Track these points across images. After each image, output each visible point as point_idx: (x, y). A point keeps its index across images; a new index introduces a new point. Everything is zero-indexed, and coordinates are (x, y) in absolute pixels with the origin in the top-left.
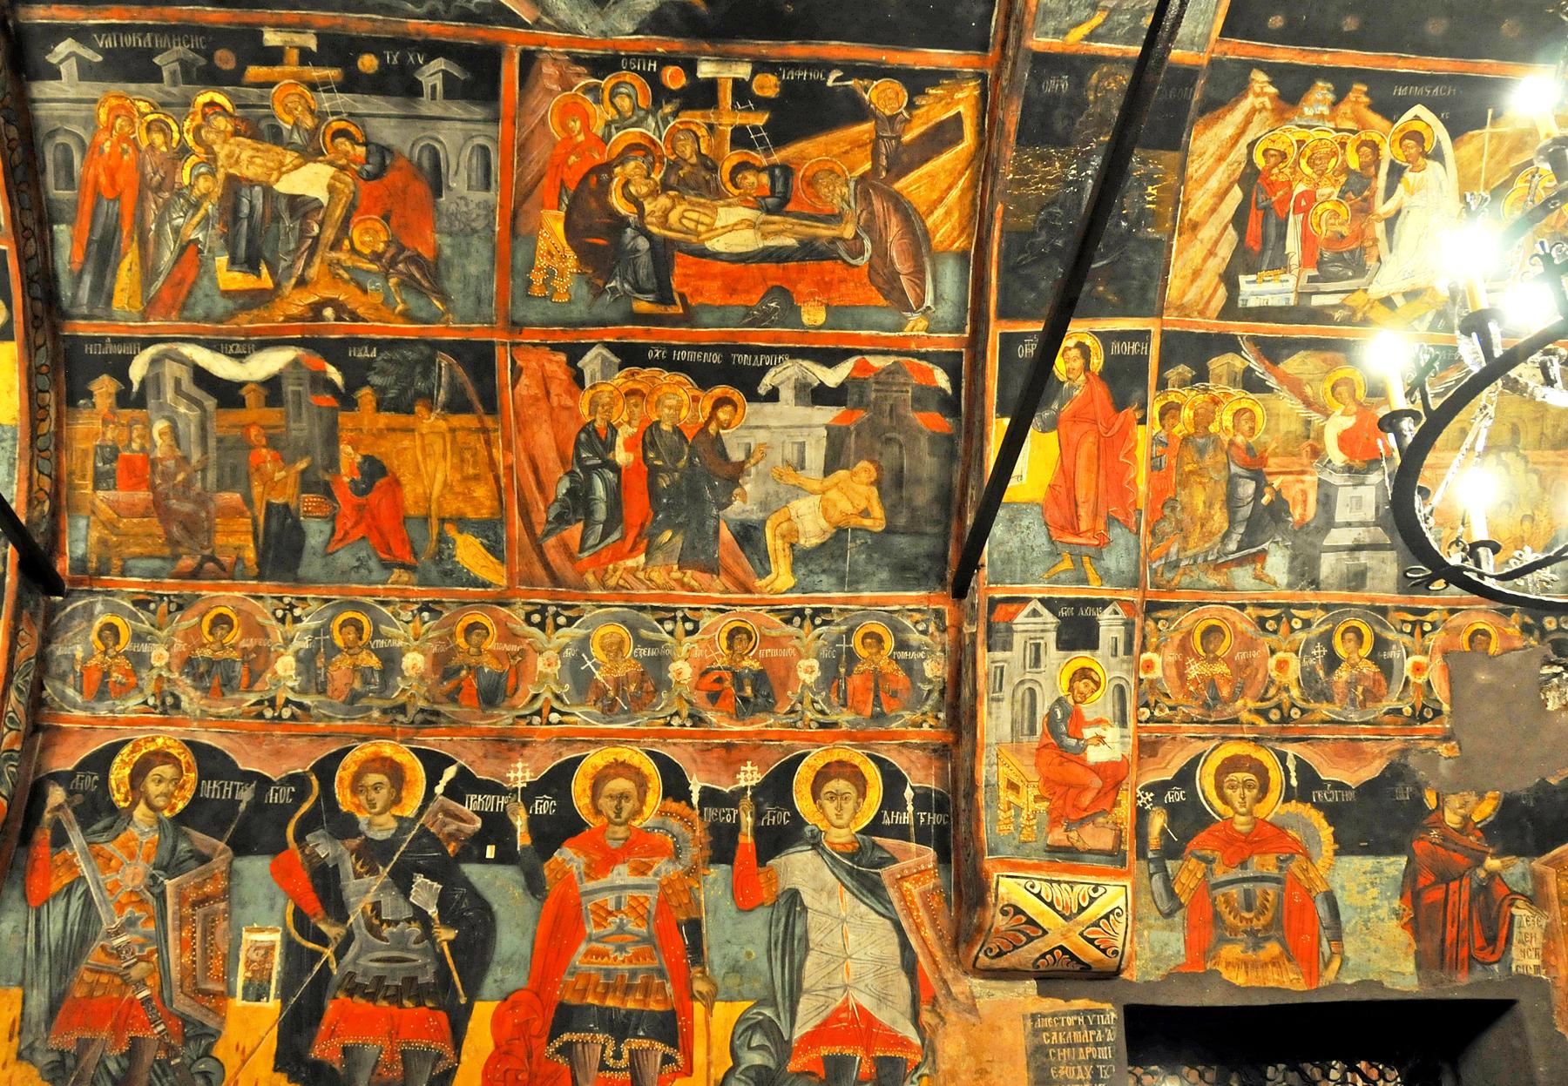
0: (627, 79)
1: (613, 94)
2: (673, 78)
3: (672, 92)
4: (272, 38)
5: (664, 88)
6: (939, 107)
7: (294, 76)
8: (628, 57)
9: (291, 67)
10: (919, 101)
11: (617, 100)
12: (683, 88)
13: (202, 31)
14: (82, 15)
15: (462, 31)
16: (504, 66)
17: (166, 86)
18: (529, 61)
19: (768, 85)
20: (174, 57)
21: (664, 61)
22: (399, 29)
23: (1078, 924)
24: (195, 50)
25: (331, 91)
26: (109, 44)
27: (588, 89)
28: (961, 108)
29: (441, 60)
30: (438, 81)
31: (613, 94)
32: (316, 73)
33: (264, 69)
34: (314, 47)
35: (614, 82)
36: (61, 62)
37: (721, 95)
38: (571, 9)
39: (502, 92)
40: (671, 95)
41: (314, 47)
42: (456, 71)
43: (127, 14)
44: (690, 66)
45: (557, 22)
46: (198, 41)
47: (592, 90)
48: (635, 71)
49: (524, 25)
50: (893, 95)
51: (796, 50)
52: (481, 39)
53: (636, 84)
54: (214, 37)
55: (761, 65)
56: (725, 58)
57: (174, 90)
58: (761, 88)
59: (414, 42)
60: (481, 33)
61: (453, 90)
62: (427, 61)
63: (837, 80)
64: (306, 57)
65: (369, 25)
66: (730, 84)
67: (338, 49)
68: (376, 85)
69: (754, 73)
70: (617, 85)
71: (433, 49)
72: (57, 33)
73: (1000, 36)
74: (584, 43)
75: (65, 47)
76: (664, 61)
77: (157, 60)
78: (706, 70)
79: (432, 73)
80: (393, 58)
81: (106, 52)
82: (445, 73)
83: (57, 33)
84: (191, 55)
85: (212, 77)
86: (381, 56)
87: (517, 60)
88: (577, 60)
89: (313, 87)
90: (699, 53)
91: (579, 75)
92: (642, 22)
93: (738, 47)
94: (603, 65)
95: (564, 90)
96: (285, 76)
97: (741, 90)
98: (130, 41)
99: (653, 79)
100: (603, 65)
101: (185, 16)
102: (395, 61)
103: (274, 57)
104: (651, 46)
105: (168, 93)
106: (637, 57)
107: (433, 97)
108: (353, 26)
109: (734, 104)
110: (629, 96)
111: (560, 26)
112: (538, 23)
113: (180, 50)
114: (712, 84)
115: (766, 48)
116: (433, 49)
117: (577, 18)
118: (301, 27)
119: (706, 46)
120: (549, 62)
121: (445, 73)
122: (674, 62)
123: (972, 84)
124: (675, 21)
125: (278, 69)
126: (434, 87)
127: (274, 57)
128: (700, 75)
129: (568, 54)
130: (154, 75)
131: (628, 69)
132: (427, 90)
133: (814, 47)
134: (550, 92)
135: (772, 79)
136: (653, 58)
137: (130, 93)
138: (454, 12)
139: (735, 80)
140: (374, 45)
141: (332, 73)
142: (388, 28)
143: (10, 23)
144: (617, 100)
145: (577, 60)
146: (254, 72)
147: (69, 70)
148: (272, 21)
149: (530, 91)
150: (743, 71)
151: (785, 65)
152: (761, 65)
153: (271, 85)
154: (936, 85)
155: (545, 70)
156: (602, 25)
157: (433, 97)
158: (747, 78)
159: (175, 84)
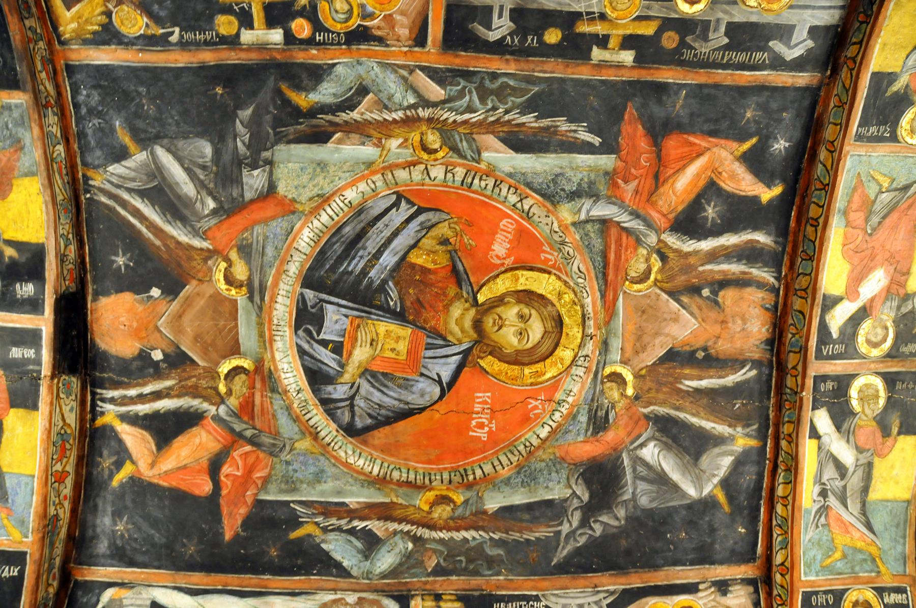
0: (339, 26)
1: (350, 11)
2: (301, 27)
3: (302, 16)
4: (628, 57)
5: (308, 19)
6: (86, 15)
7: (617, 26)
8: (339, 44)
9: (616, 34)
10: (104, 19)
11: (346, 7)
12: (293, 19)
13: (682, 63)
14: (770, 78)
15: (473, 63)
16: (440, 35)
17: (726, 19)
18: (420, 39)
19: (225, 24)
20: (710, 44)
21: (310, 42)
22: (523, 65)
23: (472, 504)
24: (692, 48)
25: (588, 13)
26: (759, 55)
27: (371, 16)
28: (68, 15)
29: (491, 39)
30: (496, 21)
31: (350, 11)
32: (599, 28)
33: (640, 32)
34: (595, 48)
35: (350, 23)
36: (805, 40)
37: (262, 14)
38: (385, 83)
39: (443, 12)
40: (302, 13)
41: (595, 48)
42: (480, 30)
43: (736, 78)
44: (290, 38)
45: (396, 72)
46: (687, 55)
47: (366, 16)
48: (333, 33)
49: (423, 69)
50: (126, 22)
51: (208, 57)
52: (457, 56)
53: (331, 21)
54: (675, 58)
55: (232, 41)
56: (261, 47)
57: (720, 15)
58: (230, 23)
59: (512, 53)
60: (458, 61)
61: (485, 14)
62: (504, 38)
63: (172, 33)
64: (603, 41)
65: (547, 67)
66: (256, 25)
67: (577, 47)
68: (549, 18)
69: (238, 35)
70: (347, 20)
71: (498, 48)
72: (798, 65)
73: (60, 79)
74: (375, 55)
75: (791, 54)
76: (310, 42)
77: (726, 40)
78: (276, 36)
79: (501, 27)
80: (531, 40)
81: (764, 48)
82: (489, 28)
83: (798, 65)
84: (696, 45)
85: (685, 26)
86: (541, 41)
87: (430, 39)
88: (381, 40)
89: (603, 17)
90: (284, 50)
91: (379, 28)
92: (330, 74)
93: (253, 57)
94: (359, 36)
95: (391, 15)
96: (624, 26)
97: (246, 20)
98: (742, 57)
99: (318, 26)
100: (359, 36)
101: (691, 75)
102: (530, 38)
103: (629, 42)
104: (321, 54)
105: (725, 12)
106: (332, 44)
107: (502, 7)
108: (561, 67)
109: (250, 8)
110: (337, 12)
111: (394, 68)
112: (411, 72)
113: (703, 49)
114: (271, 23)
115: (232, 57)
116: (498, 48)
117: (381, 76)
118: (603, 65)
119: (278, 57)
120: (403, 38)
121: (489, 28)
122: (302, 42)
123: (67, 36)
124: (304, 75)
125: (628, 32)
126: (500, 16)
127: (629, 42)
128: (281, 31)
129: (387, 46)
130: (733, 29)
131: (339, 34)
132: (506, 14)
133: (194, 60)
134: (403, 13)
135: (223, 31)
136: (319, 44)
137: (759, 13)
138: (477, 79)
139: (251, 27)
140: (546, 51)
141: (583, 28)
142: (532, 66)
143: (829, 72)
144: (346, 7)
145: (381, 40)
146: (648, 29)
147: (801, 34)
148: (623, 72)
149: (419, 13)
150: (247, 36)
151: (215, 44)
152: (232, 41)
153: (639, 18)
154: (94, 33)
155: (407, 32)
156: (361, 70)
157: (502, 7)
158: (243, 30)
159: (718, 21)
